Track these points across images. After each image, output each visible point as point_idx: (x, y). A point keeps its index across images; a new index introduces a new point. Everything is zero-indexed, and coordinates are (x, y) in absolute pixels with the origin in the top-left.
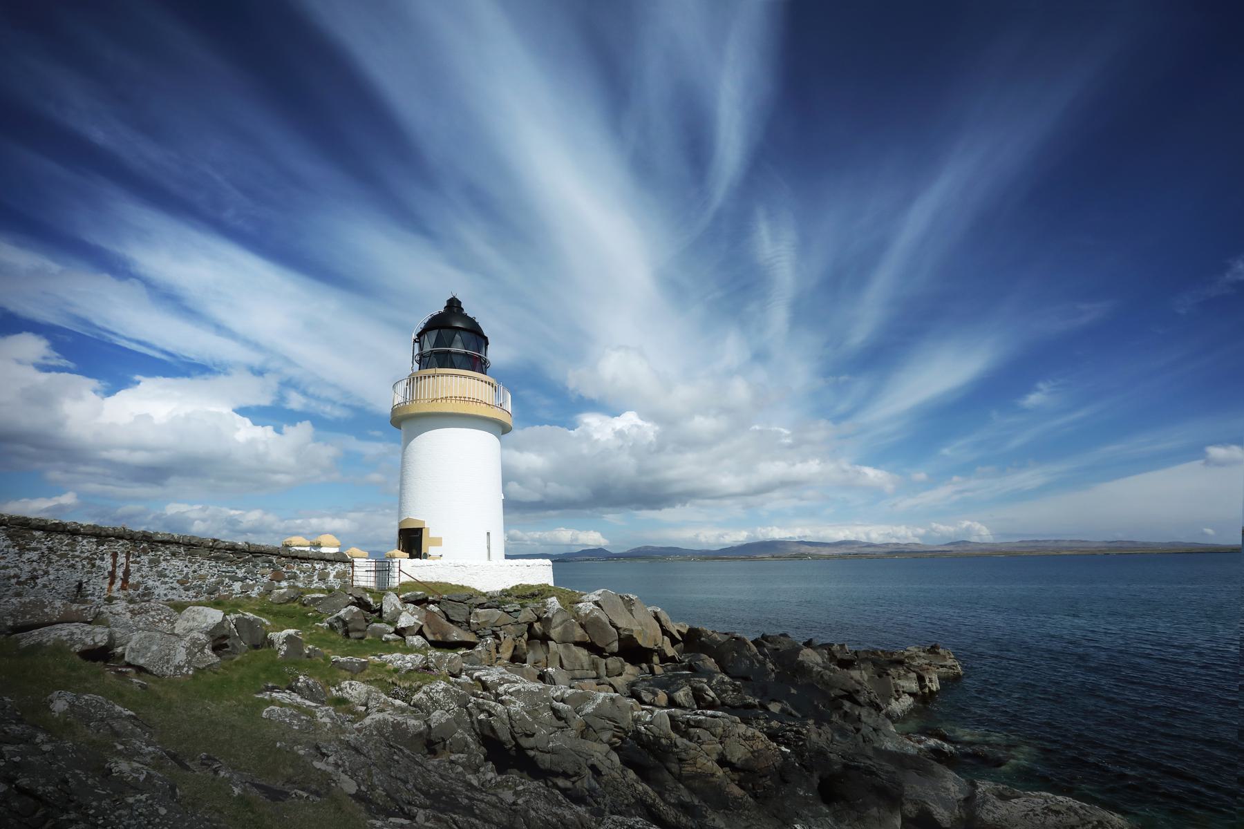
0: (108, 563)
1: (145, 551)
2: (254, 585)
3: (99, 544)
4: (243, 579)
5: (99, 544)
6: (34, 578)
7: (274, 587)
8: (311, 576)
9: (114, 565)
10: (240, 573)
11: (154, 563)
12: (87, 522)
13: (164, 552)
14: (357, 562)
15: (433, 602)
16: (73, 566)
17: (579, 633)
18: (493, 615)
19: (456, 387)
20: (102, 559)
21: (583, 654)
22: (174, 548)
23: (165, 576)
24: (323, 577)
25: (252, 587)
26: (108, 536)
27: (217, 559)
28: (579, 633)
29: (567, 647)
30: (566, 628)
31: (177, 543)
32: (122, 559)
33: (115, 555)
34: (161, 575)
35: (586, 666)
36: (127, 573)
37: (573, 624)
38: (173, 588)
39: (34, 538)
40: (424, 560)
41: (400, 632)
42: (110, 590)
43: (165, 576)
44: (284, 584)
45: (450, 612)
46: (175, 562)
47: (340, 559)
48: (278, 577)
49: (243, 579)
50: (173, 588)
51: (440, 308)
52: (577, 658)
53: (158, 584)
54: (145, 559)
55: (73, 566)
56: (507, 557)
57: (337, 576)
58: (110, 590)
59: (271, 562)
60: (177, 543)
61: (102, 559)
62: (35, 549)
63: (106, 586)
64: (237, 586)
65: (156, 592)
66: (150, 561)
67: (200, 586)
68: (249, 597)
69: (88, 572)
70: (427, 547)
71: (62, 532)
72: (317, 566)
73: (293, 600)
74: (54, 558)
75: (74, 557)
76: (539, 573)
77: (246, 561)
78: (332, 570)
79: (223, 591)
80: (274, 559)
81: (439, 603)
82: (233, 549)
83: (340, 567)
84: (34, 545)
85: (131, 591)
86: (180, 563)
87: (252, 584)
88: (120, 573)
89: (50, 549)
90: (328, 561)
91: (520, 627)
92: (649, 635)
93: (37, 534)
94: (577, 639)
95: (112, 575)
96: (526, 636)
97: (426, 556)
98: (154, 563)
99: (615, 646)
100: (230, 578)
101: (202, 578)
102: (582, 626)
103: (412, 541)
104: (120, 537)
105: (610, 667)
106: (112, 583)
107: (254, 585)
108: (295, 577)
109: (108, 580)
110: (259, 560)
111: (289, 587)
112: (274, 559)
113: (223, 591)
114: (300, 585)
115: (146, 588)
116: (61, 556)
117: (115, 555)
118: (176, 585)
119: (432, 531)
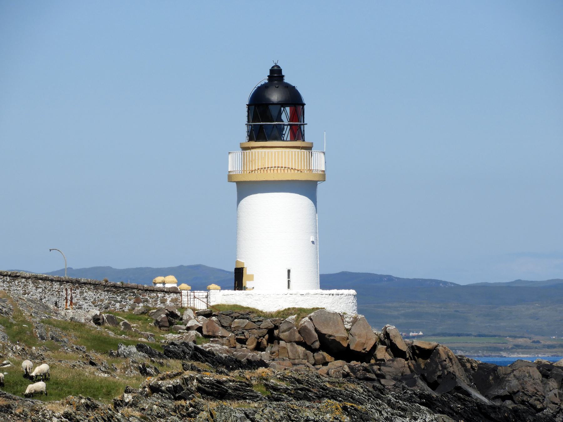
0: (64, 293)
1: (77, 288)
2: (126, 305)
3: (61, 285)
4: (120, 302)
5: (61, 285)
6: (41, 299)
7: (136, 306)
8: (156, 301)
9: (67, 294)
10: (119, 299)
11: (82, 293)
12: (133, 284)
13: (85, 289)
14: (184, 292)
15: (215, 315)
16: (53, 294)
17: (297, 336)
18: (244, 323)
19: (276, 158)
20: (62, 292)
21: (301, 349)
22: (89, 286)
23: (86, 300)
24: (163, 301)
25: (125, 306)
26: (63, 281)
27: (108, 291)
28: (297, 336)
29: (292, 345)
30: (291, 334)
31: (90, 284)
32: (69, 292)
33: (66, 290)
34: (85, 299)
35: (301, 356)
36: (72, 298)
37: (294, 330)
38: (90, 306)
39: (39, 283)
40: (243, 291)
41: (188, 329)
42: (66, 305)
43: (86, 300)
44: (141, 305)
45: (222, 321)
46: (90, 293)
47: (175, 291)
48: (138, 301)
49: (120, 302)
50: (90, 306)
51: (263, 78)
52: (297, 351)
53: (84, 303)
54: (78, 291)
55: (53, 294)
56: (324, 286)
57: (172, 301)
58: (66, 305)
59: (134, 293)
60: (90, 284)
61: (62, 292)
62: (40, 288)
63: (65, 304)
64: (118, 305)
65: (83, 307)
66: (80, 293)
67: (101, 305)
68: (123, 311)
69: (59, 298)
70: (247, 283)
71: (48, 280)
72: (159, 295)
73: (143, 313)
74: (47, 291)
75: (53, 291)
76: (341, 302)
77: (121, 292)
78: (169, 298)
79: (111, 308)
80: (136, 291)
81: (217, 316)
82: (115, 286)
83: (173, 296)
84: (40, 286)
85: (74, 306)
86: (92, 293)
87: (123, 305)
88: (69, 298)
89: (45, 287)
90: (166, 292)
91: (261, 331)
92: (402, 345)
93: (40, 281)
94: (297, 340)
95: (66, 298)
96: (267, 336)
97: (245, 288)
98: (82, 293)
99: (317, 345)
100: (115, 301)
101: (102, 301)
102: (299, 332)
103: (238, 279)
104: (67, 282)
105: (316, 358)
106: (67, 302)
107: (126, 305)
108: (147, 301)
109: (65, 301)
110: (128, 292)
111: (144, 306)
112: (136, 291)
113: (111, 308)
114: (150, 305)
115: (79, 305)
116: (49, 290)
117: (66, 290)
118: (91, 304)
119: (248, 272)
